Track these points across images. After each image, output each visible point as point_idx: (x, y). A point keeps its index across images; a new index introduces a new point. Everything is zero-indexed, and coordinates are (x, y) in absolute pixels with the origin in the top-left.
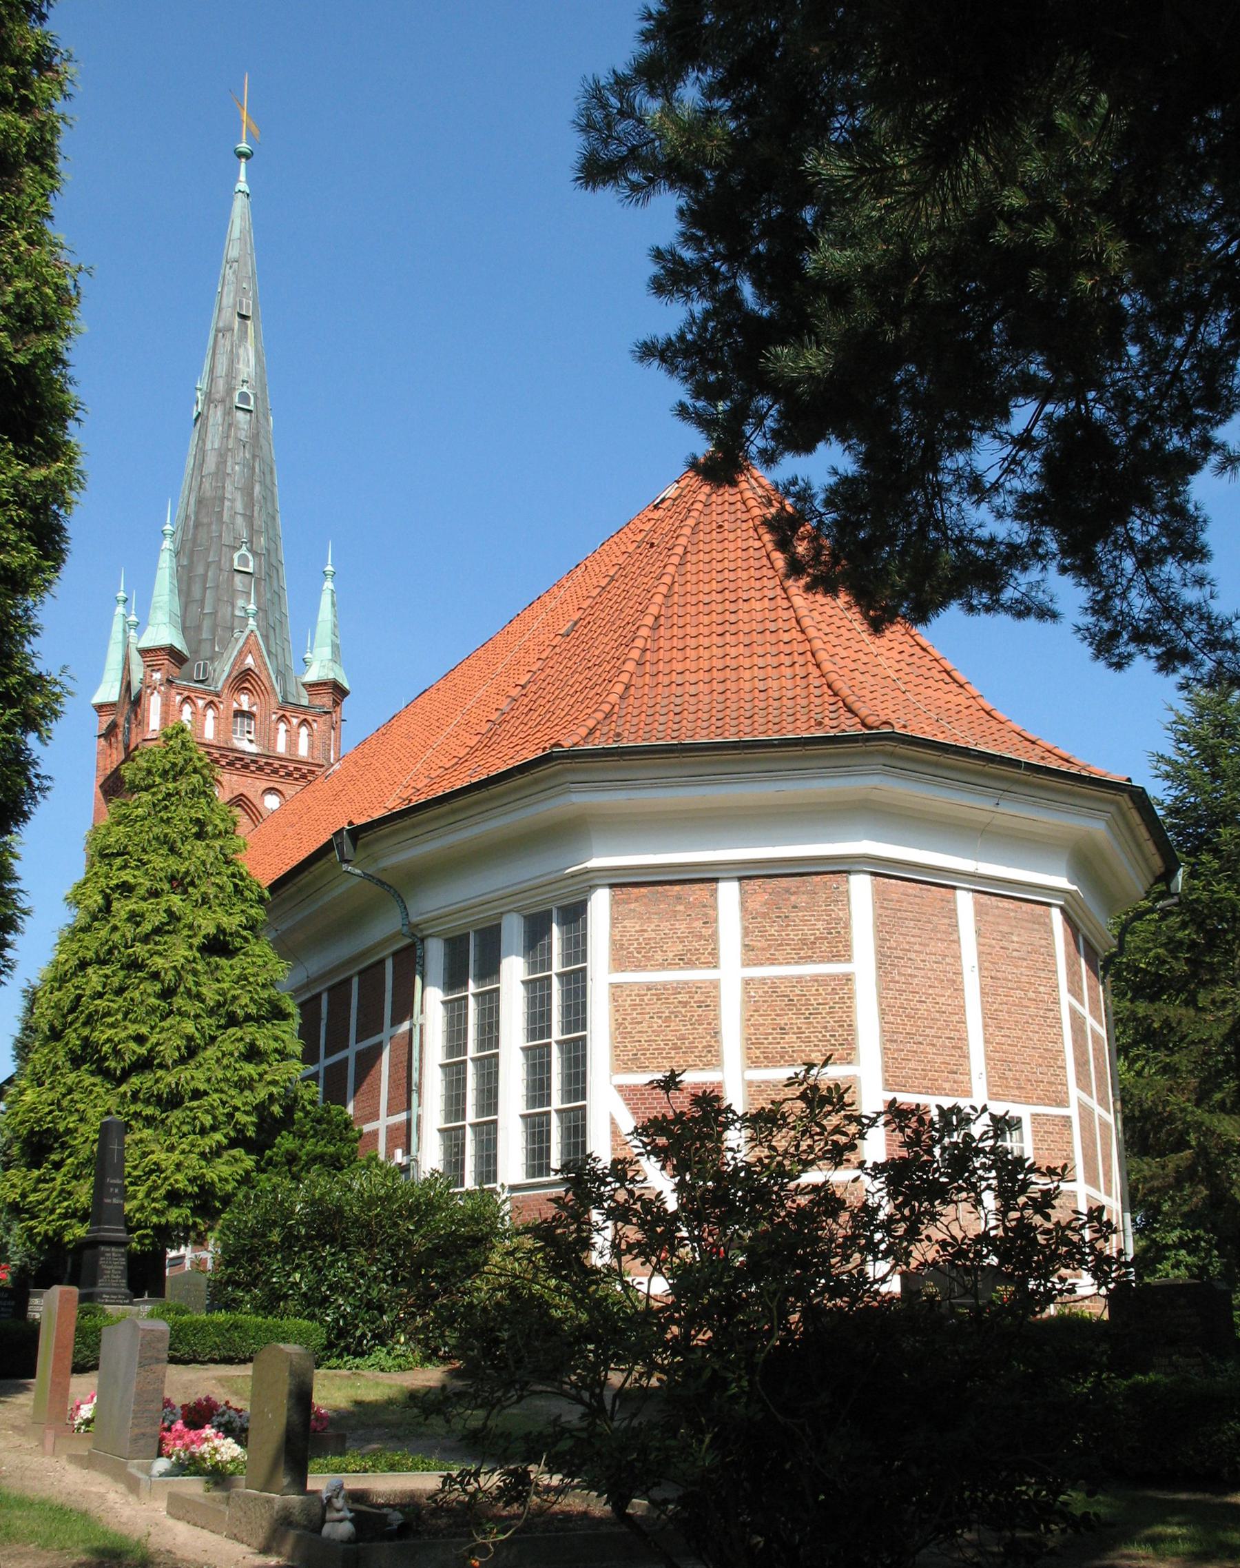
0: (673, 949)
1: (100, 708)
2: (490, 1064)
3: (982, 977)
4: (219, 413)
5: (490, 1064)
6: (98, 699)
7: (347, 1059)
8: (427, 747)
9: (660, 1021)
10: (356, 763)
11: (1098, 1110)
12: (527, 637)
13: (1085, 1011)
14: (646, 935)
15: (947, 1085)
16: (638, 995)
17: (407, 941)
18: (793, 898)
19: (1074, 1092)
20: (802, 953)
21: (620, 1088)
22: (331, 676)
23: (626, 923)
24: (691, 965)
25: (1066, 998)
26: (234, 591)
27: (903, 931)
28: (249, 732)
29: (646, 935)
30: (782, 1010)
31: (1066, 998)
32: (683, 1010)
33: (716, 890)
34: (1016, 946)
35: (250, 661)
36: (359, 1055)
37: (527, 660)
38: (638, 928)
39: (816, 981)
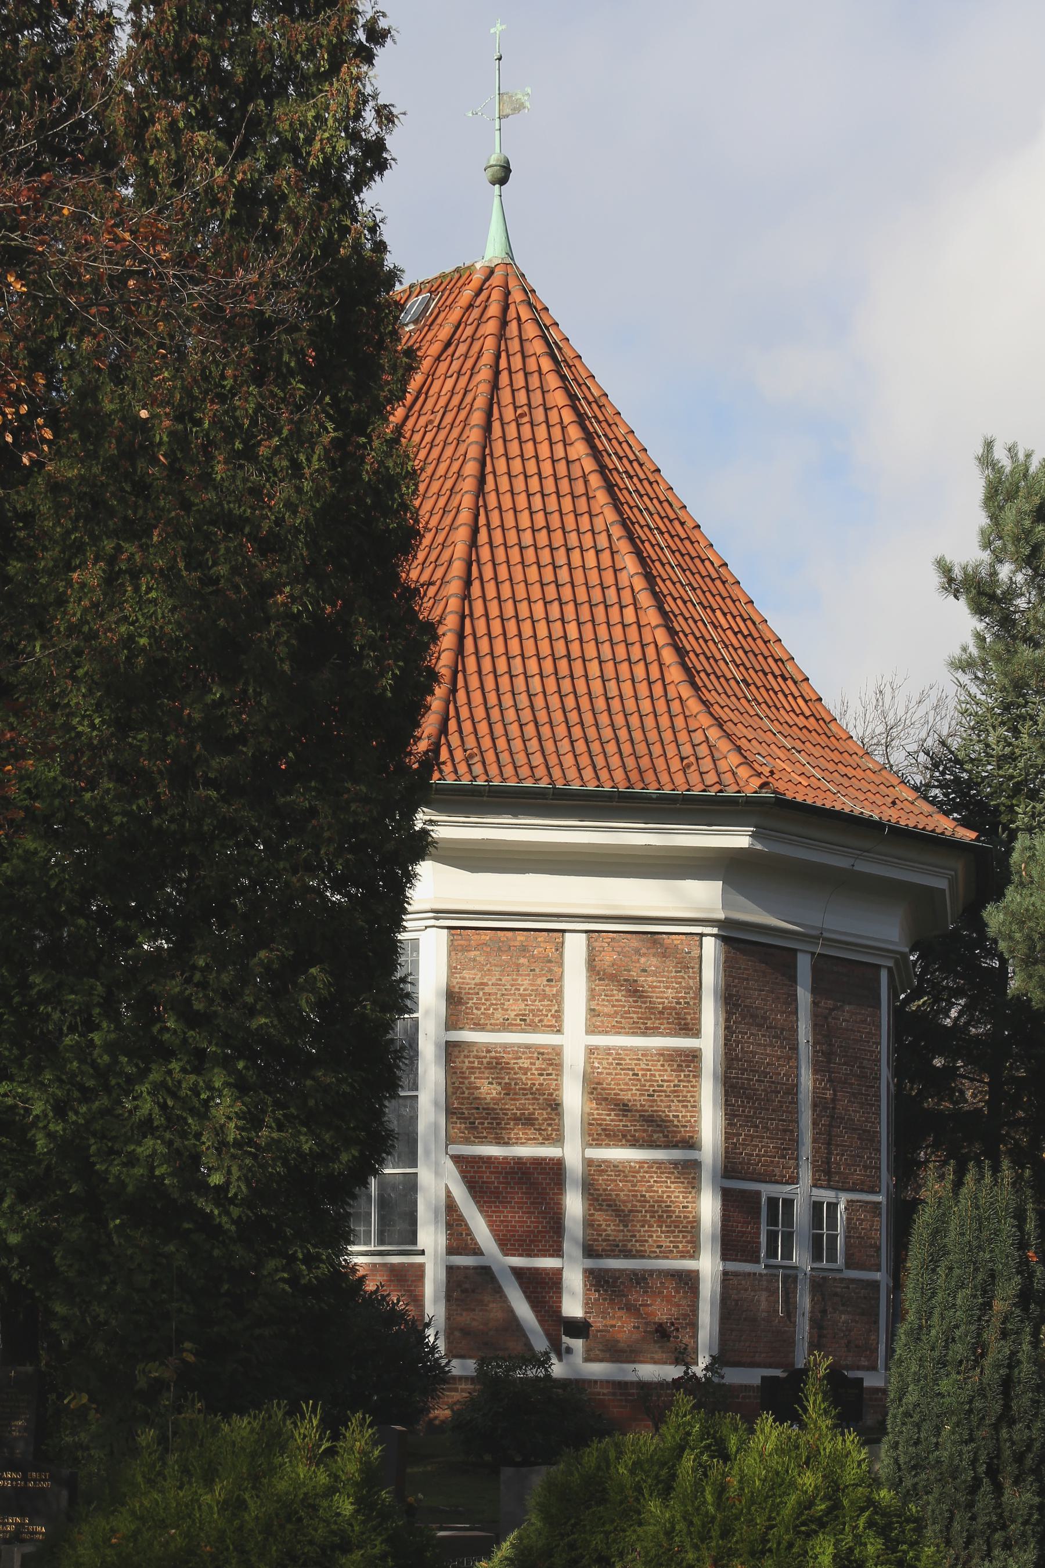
16: (477, 1057)
18: (643, 960)
21: (457, 1159)
23: (465, 973)
29: (487, 990)
32: (524, 1077)
38: (477, 981)
39: (662, 1055)
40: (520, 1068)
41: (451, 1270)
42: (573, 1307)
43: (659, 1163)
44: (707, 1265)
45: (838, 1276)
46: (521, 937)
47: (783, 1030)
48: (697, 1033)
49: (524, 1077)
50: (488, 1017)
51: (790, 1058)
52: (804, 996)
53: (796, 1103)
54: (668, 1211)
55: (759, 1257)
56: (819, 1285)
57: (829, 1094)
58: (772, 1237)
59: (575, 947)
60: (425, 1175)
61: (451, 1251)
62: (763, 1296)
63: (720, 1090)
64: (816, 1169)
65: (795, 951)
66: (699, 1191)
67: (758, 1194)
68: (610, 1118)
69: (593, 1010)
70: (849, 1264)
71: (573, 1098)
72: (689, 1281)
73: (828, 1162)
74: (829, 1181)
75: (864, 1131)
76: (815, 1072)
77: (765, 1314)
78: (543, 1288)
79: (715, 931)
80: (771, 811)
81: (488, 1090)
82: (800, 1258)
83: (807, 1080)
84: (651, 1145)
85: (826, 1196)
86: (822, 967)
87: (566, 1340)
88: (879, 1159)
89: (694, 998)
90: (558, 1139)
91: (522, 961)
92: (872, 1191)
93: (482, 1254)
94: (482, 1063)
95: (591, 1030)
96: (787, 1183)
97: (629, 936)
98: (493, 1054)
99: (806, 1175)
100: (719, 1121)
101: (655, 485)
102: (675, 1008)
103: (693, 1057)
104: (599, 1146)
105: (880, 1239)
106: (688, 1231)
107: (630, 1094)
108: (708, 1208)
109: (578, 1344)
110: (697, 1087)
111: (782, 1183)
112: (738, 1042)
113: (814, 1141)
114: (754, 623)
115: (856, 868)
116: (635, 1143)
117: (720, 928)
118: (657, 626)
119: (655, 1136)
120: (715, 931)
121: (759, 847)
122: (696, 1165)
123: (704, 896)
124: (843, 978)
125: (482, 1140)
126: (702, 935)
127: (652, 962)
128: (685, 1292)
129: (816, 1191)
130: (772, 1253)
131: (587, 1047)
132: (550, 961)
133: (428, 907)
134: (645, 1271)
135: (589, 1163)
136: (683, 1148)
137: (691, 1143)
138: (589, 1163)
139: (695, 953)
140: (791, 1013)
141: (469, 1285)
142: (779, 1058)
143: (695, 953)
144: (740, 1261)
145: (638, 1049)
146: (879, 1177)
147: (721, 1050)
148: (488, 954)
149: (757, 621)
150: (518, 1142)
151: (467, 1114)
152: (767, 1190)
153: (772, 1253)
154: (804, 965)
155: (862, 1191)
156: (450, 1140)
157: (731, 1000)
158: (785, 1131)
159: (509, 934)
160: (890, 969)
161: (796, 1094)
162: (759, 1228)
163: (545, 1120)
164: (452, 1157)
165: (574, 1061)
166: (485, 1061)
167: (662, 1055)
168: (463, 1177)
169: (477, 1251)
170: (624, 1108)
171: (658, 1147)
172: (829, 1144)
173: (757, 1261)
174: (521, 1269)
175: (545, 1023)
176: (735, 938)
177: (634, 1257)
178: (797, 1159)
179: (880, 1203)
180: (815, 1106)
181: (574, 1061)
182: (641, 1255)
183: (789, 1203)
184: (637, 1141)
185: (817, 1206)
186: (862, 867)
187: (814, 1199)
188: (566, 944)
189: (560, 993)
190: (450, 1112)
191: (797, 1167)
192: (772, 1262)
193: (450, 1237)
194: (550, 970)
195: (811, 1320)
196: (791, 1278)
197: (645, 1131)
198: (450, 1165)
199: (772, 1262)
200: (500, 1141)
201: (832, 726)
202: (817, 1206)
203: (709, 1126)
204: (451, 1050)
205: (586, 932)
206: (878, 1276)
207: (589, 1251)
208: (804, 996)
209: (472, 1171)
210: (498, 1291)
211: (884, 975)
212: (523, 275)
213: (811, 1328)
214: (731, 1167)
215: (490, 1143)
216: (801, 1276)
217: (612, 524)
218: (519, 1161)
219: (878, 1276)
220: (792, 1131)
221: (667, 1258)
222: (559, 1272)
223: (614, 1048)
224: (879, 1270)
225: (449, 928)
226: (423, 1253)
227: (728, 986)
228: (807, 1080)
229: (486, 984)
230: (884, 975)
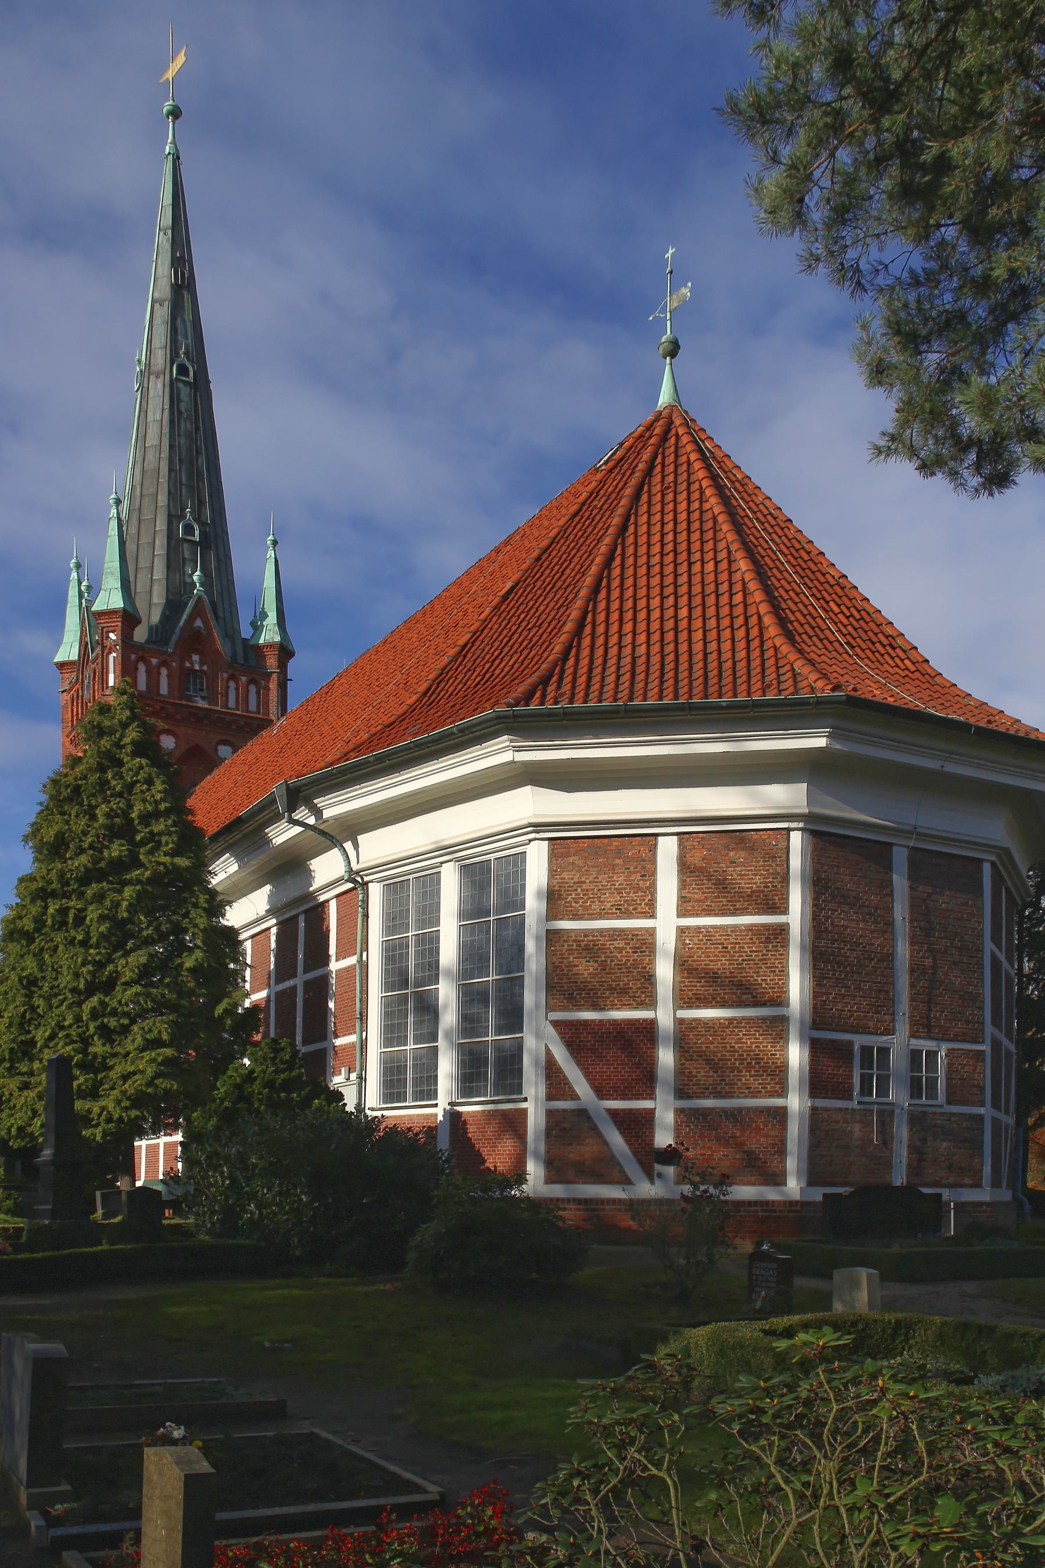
0: (610, 900)
1: (62, 666)
2: (431, 880)
3: (912, 927)
4: (160, 386)
5: (431, 880)
6: (58, 658)
7: (305, 972)
8: (366, 704)
9: (596, 965)
10: (300, 718)
11: (1005, 1042)
12: (465, 600)
13: (1002, 957)
14: (584, 886)
16: (576, 941)
17: (350, 885)
18: (731, 854)
19: (989, 1028)
20: (738, 905)
21: (556, 1024)
22: (1007, 846)
23: (565, 875)
24: (628, 915)
25: (988, 946)
26: (184, 558)
28: (202, 690)
29: (584, 886)
30: (716, 956)
31: (988, 946)
32: (619, 955)
33: (656, 845)
35: (199, 623)
36: (307, 984)
37: (465, 622)
38: (576, 880)
39: (751, 930)
40: (615, 948)
41: (550, 1113)
42: (663, 1139)
43: (748, 1020)
44: (795, 1102)
45: (938, 1110)
46: (616, 843)
47: (876, 909)
48: (785, 911)
49: (619, 955)
50: (586, 908)
51: (885, 932)
52: (900, 882)
53: (892, 968)
54: (758, 1060)
55: (852, 1095)
56: (917, 1120)
57: (929, 962)
58: (866, 1081)
59: (667, 849)
60: (530, 1042)
61: (550, 1097)
62: (857, 1127)
63: (808, 957)
64: (913, 1023)
65: (890, 845)
66: (787, 1041)
67: (850, 1043)
68: (700, 987)
69: (685, 897)
70: (949, 1102)
71: (664, 971)
72: (780, 1115)
73: (928, 1018)
74: (929, 1032)
75: (966, 993)
76: (912, 943)
77: (857, 1143)
78: (638, 1126)
79: (801, 825)
80: (848, 711)
81: (585, 969)
82: (897, 1095)
83: (903, 950)
84: (740, 1004)
85: (925, 1045)
86: (918, 860)
87: (658, 1167)
88: (983, 1016)
89: (782, 882)
90: (651, 1002)
91: (617, 861)
92: (975, 1041)
93: (579, 1099)
94: (580, 946)
95: (682, 913)
96: (882, 1034)
97: (718, 835)
98: (591, 938)
99: (903, 1028)
100: (807, 983)
101: (786, 530)
102: (763, 891)
103: (782, 930)
104: (690, 1007)
105: (984, 1080)
106: (776, 1075)
107: (721, 964)
108: (796, 1055)
109: (670, 1170)
110: (785, 957)
111: (875, 1034)
112: (827, 918)
113: (912, 1000)
114: (869, 614)
115: (945, 769)
116: (723, 1004)
117: (806, 822)
118: (761, 602)
119: (744, 997)
120: (801, 825)
121: (838, 747)
122: (784, 1020)
123: (784, 796)
124: (942, 869)
125: (580, 1008)
126: (789, 830)
127: (740, 856)
128: (774, 1126)
129: (913, 1041)
130: (865, 1090)
131: (678, 927)
132: (644, 860)
133: (525, 822)
134: (734, 1109)
135: (680, 1022)
136: (772, 1006)
137: (780, 1000)
138: (680, 1022)
139: (782, 844)
140: (885, 895)
141: (567, 1127)
142: (872, 932)
143: (782, 844)
144: (830, 1098)
145: (728, 926)
146: (983, 1030)
147: (808, 924)
148: (585, 858)
149: (871, 611)
150: (613, 1007)
151: (562, 987)
152: (858, 1041)
153: (865, 1090)
154: (900, 857)
155: (964, 1041)
156: (549, 1008)
157: (819, 885)
158: (879, 991)
159: (606, 841)
160: (993, 864)
161: (892, 961)
162: (851, 1071)
163: (639, 988)
164: (551, 1022)
165: (666, 938)
166: (583, 944)
167: (751, 930)
168: (562, 1038)
169: (575, 1097)
170: (713, 977)
171: (747, 1006)
172: (929, 1002)
173: (850, 1098)
174: (616, 1110)
175: (639, 910)
176: (822, 834)
177: (724, 1097)
178: (893, 1014)
179: (984, 1051)
180: (912, 971)
181: (666, 938)
182: (729, 1095)
183: (884, 1052)
184: (726, 1002)
185: (915, 1054)
186: (951, 768)
187: (911, 1047)
188: (659, 847)
189: (654, 885)
190: (550, 987)
191: (893, 1020)
192: (867, 1099)
193: (549, 1086)
194: (644, 868)
195: (909, 1146)
196: (887, 1115)
197: (735, 993)
198: (551, 1030)
199: (867, 1099)
200: (596, 1007)
201: (937, 679)
202: (915, 1054)
203: (797, 987)
204: (552, 937)
205: (677, 834)
206: (982, 1111)
207: (681, 1093)
208: (900, 882)
209: (574, 1036)
210: (595, 1129)
211: (987, 868)
212: (686, 412)
213: (909, 1153)
214: (820, 1018)
215: (588, 1010)
216: (897, 1111)
217: (732, 542)
218: (615, 1023)
219: (982, 1111)
220: (887, 992)
221: (756, 1097)
222: (651, 1112)
223: (704, 927)
224: (983, 1105)
225: (549, 839)
226: (525, 1100)
227: (816, 871)
228: (903, 950)
229: (585, 882)
230: (987, 868)
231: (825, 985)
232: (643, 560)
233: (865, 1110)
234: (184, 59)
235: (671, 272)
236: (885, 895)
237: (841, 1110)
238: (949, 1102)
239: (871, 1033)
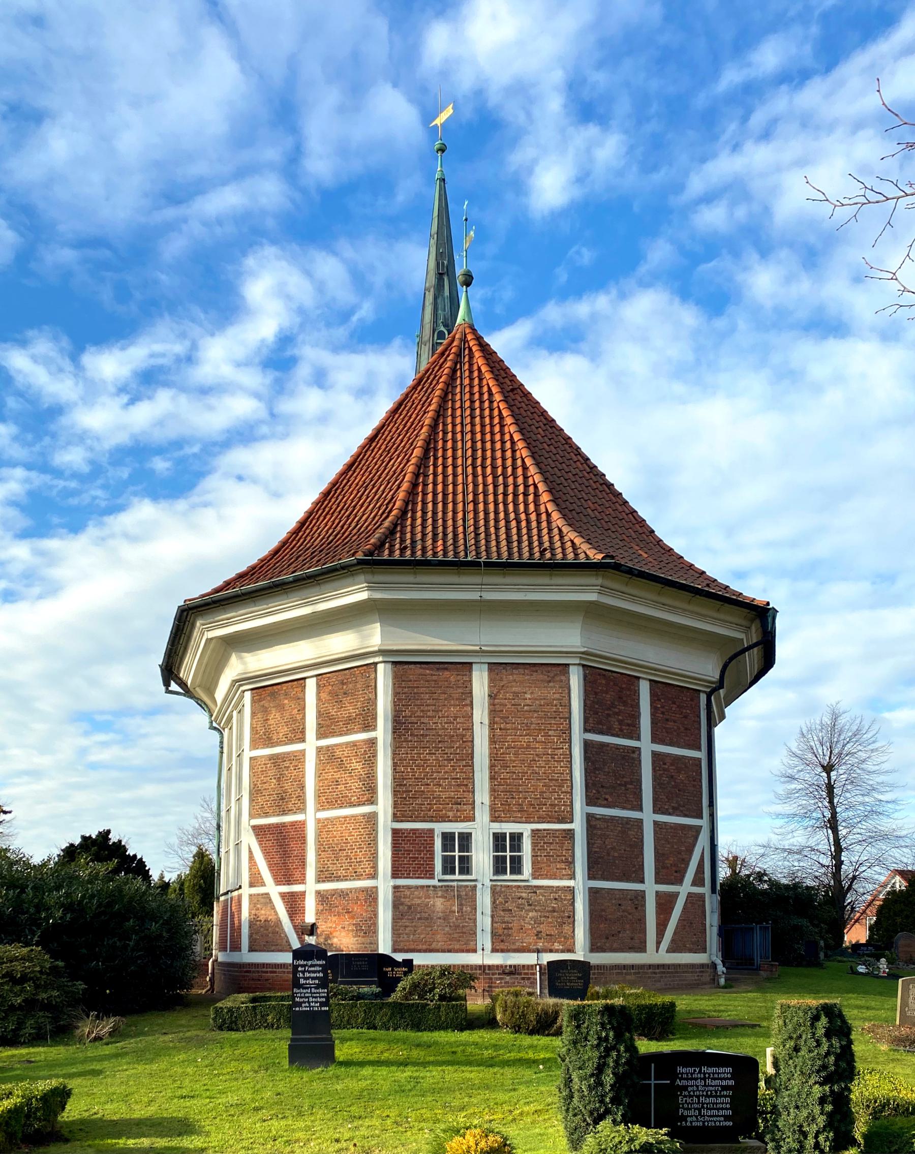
15: (450, 814)
27: (418, 702)
34: (528, 702)
46: (284, 687)
47: (455, 718)
123: (374, 636)
126: (376, 664)
131: (317, 748)
144: (412, 878)
152: (440, 828)
216: (479, 886)
231: (405, 785)
232: (488, 437)
233: (445, 886)
234: (451, 111)
235: (466, 220)
236: (466, 705)
237: (422, 887)
238: (535, 876)
239: (451, 821)
